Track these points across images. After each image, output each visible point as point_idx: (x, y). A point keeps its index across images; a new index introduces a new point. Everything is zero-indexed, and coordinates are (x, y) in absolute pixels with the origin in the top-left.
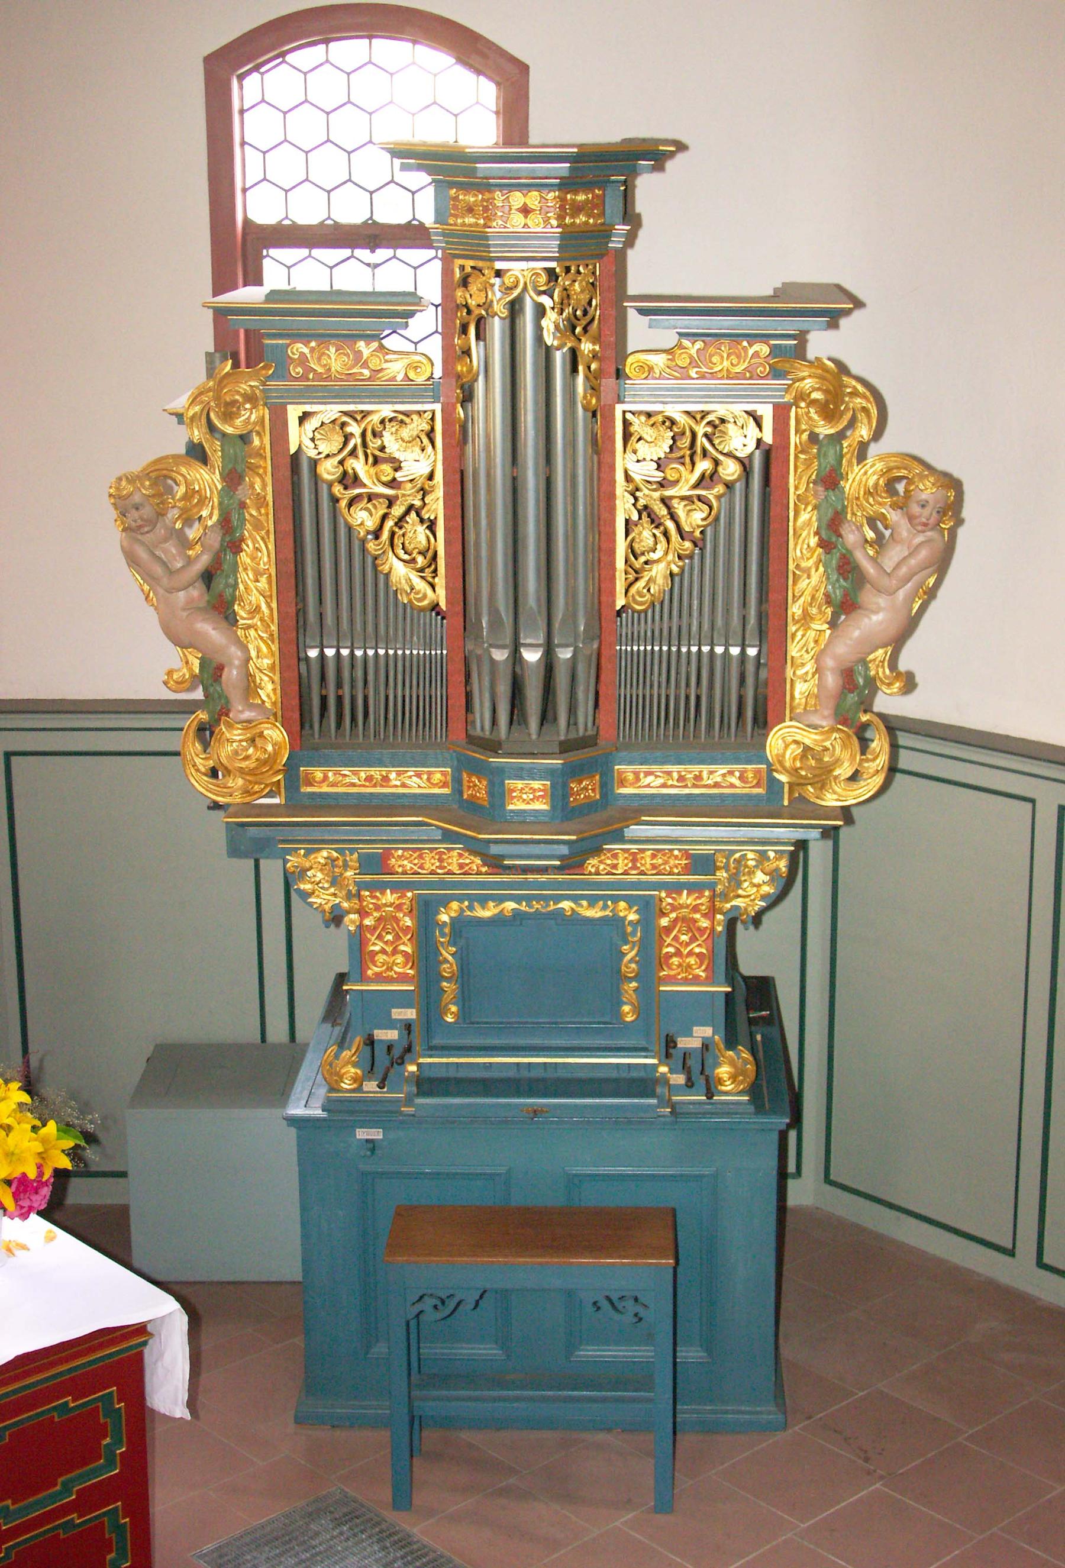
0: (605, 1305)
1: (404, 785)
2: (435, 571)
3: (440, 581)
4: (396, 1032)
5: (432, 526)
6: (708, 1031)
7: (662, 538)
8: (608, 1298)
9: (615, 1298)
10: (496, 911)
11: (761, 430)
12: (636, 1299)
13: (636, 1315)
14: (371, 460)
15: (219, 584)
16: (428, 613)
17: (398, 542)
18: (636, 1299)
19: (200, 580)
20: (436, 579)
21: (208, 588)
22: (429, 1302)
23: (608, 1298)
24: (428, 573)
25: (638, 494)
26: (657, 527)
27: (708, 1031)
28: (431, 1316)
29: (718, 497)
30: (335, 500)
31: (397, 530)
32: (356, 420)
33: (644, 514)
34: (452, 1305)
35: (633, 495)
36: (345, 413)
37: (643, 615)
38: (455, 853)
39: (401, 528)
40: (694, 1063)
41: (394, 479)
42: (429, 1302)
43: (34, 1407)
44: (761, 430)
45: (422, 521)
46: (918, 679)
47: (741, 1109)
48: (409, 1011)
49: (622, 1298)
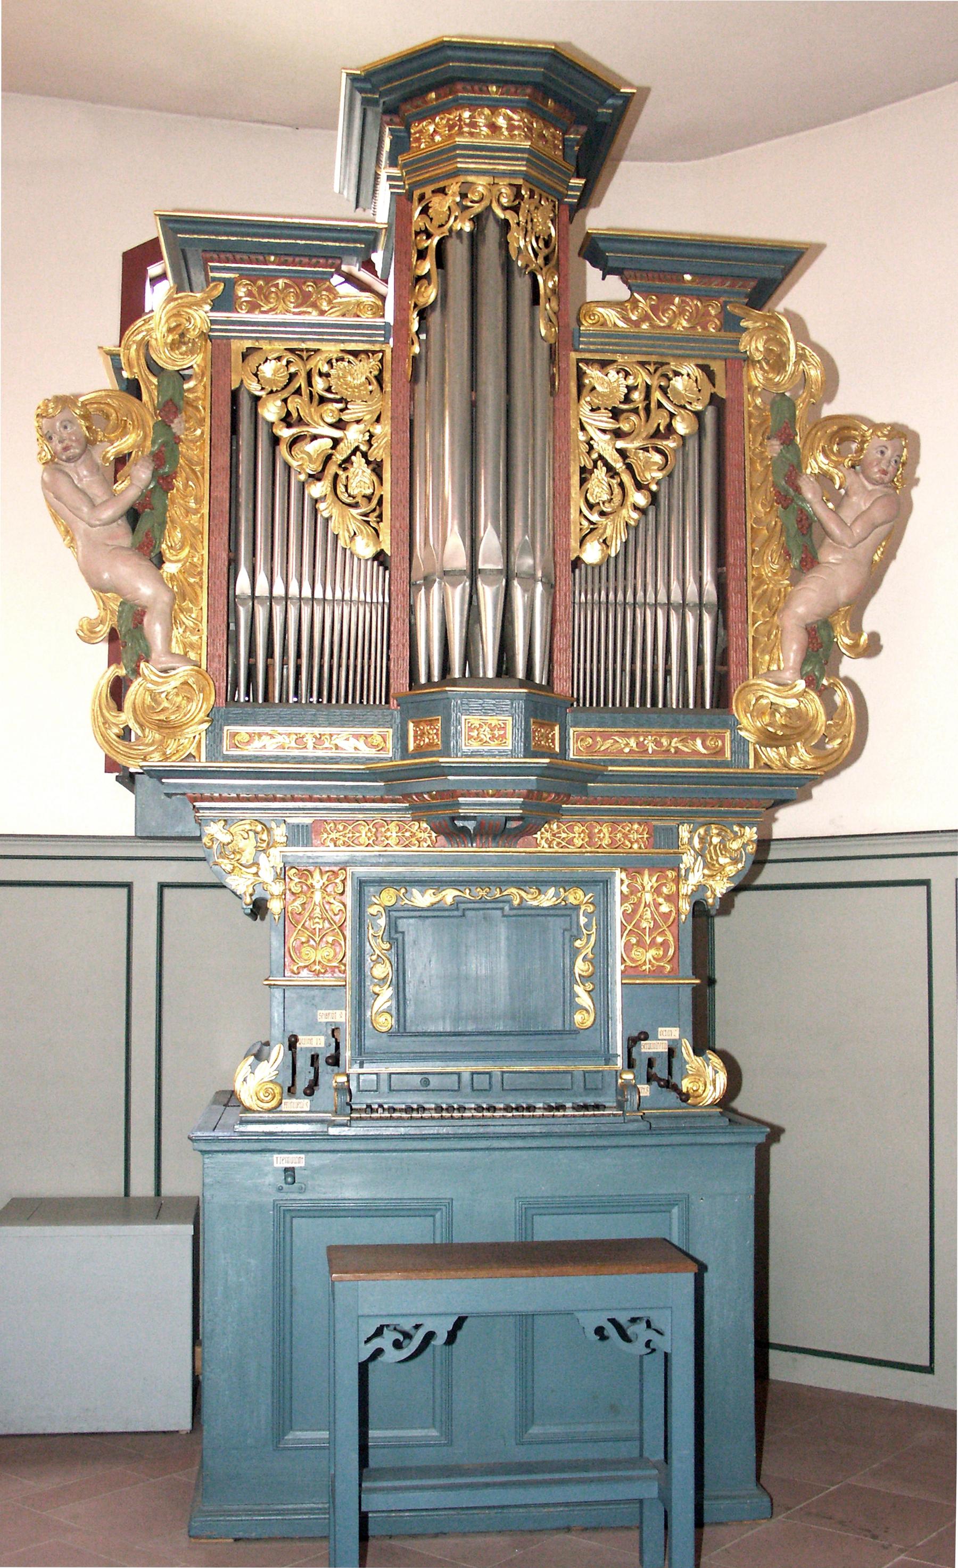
0: (611, 1330)
1: (337, 747)
2: (380, 517)
3: (385, 528)
4: (322, 1038)
5: (377, 468)
6: (674, 1033)
7: (617, 490)
8: (613, 1321)
9: (623, 1319)
10: (434, 899)
11: (714, 385)
12: (649, 1325)
13: (648, 1344)
14: (316, 398)
15: (144, 525)
16: (369, 563)
17: (341, 488)
18: (649, 1325)
19: (124, 518)
20: (381, 524)
21: (133, 529)
22: (389, 1337)
23: (613, 1321)
24: (372, 518)
25: (592, 442)
26: (612, 477)
27: (674, 1033)
28: (392, 1355)
29: (675, 450)
30: (275, 441)
31: (340, 472)
32: (301, 357)
33: (600, 463)
34: (419, 1337)
35: (588, 444)
36: (292, 351)
37: (597, 571)
38: (392, 826)
39: (345, 469)
40: (660, 1070)
41: (340, 420)
42: (389, 1337)
43: (481, 151)
44: (714, 385)
45: (368, 463)
46: (883, 642)
47: (712, 1122)
48: (338, 1012)
49: (634, 1320)
